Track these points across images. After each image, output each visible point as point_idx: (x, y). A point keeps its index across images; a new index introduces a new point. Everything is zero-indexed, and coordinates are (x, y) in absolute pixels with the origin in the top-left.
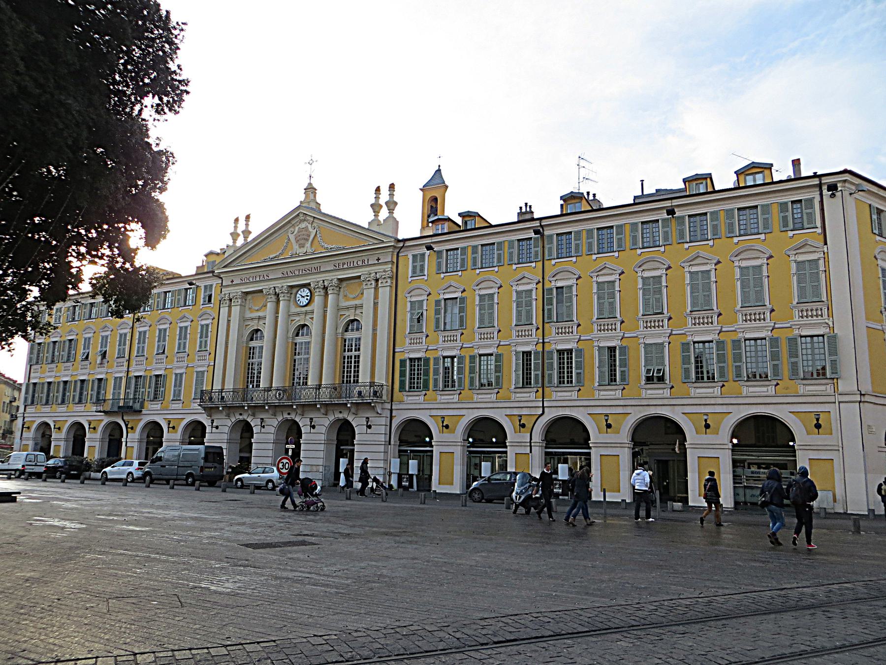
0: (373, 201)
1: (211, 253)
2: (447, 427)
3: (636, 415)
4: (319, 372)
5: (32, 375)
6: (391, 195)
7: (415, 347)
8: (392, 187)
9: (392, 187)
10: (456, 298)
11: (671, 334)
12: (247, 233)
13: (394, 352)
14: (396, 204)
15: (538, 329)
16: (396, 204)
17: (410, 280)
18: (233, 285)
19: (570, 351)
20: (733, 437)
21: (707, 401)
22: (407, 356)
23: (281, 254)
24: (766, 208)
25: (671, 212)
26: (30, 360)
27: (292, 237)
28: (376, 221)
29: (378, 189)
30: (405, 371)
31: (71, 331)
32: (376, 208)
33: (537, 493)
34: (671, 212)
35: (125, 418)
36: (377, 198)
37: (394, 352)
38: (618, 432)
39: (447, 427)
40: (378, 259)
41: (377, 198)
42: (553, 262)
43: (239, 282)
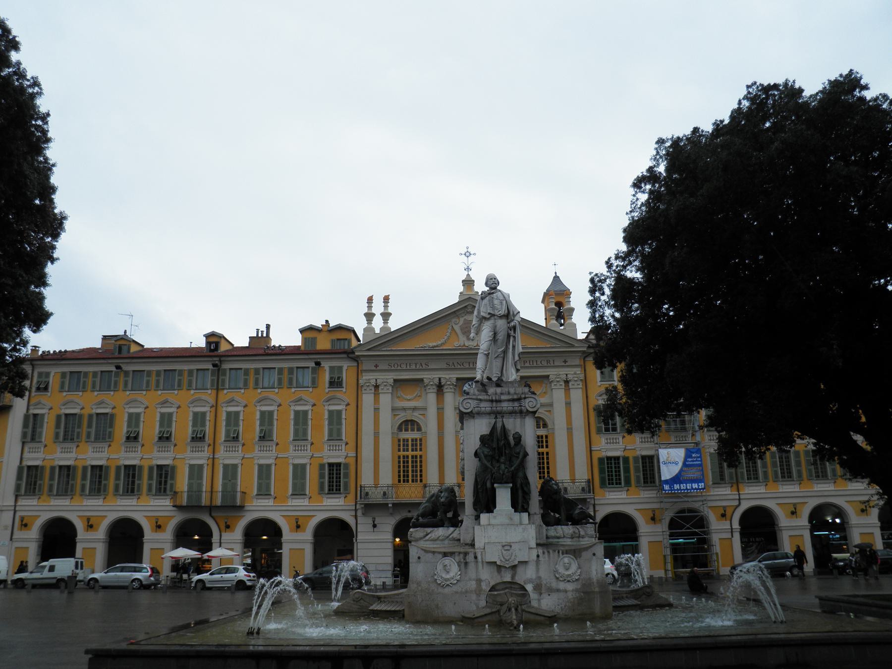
0: (366, 310)
1: (311, 329)
2: (26, 525)
3: (112, 517)
4: (377, 472)
5: (26, 455)
6: (386, 307)
7: (299, 453)
8: (386, 299)
9: (386, 299)
10: (75, 414)
11: (312, 457)
12: (386, 316)
13: (591, 451)
14: (390, 314)
15: (209, 445)
16: (390, 314)
17: (599, 384)
18: (376, 369)
19: (339, 465)
20: (395, 537)
21: (96, 508)
22: (325, 461)
23: (442, 344)
24: (281, 370)
25: (318, 364)
26: (24, 435)
27: (457, 328)
28: (368, 330)
29: (370, 300)
30: (625, 472)
31: (102, 402)
32: (369, 316)
33: (263, 586)
34: (118, 367)
35: (213, 514)
36: (370, 307)
37: (591, 451)
38: (304, 531)
39: (26, 525)
40: (565, 362)
41: (370, 307)
42: (225, 391)
43: (386, 367)
